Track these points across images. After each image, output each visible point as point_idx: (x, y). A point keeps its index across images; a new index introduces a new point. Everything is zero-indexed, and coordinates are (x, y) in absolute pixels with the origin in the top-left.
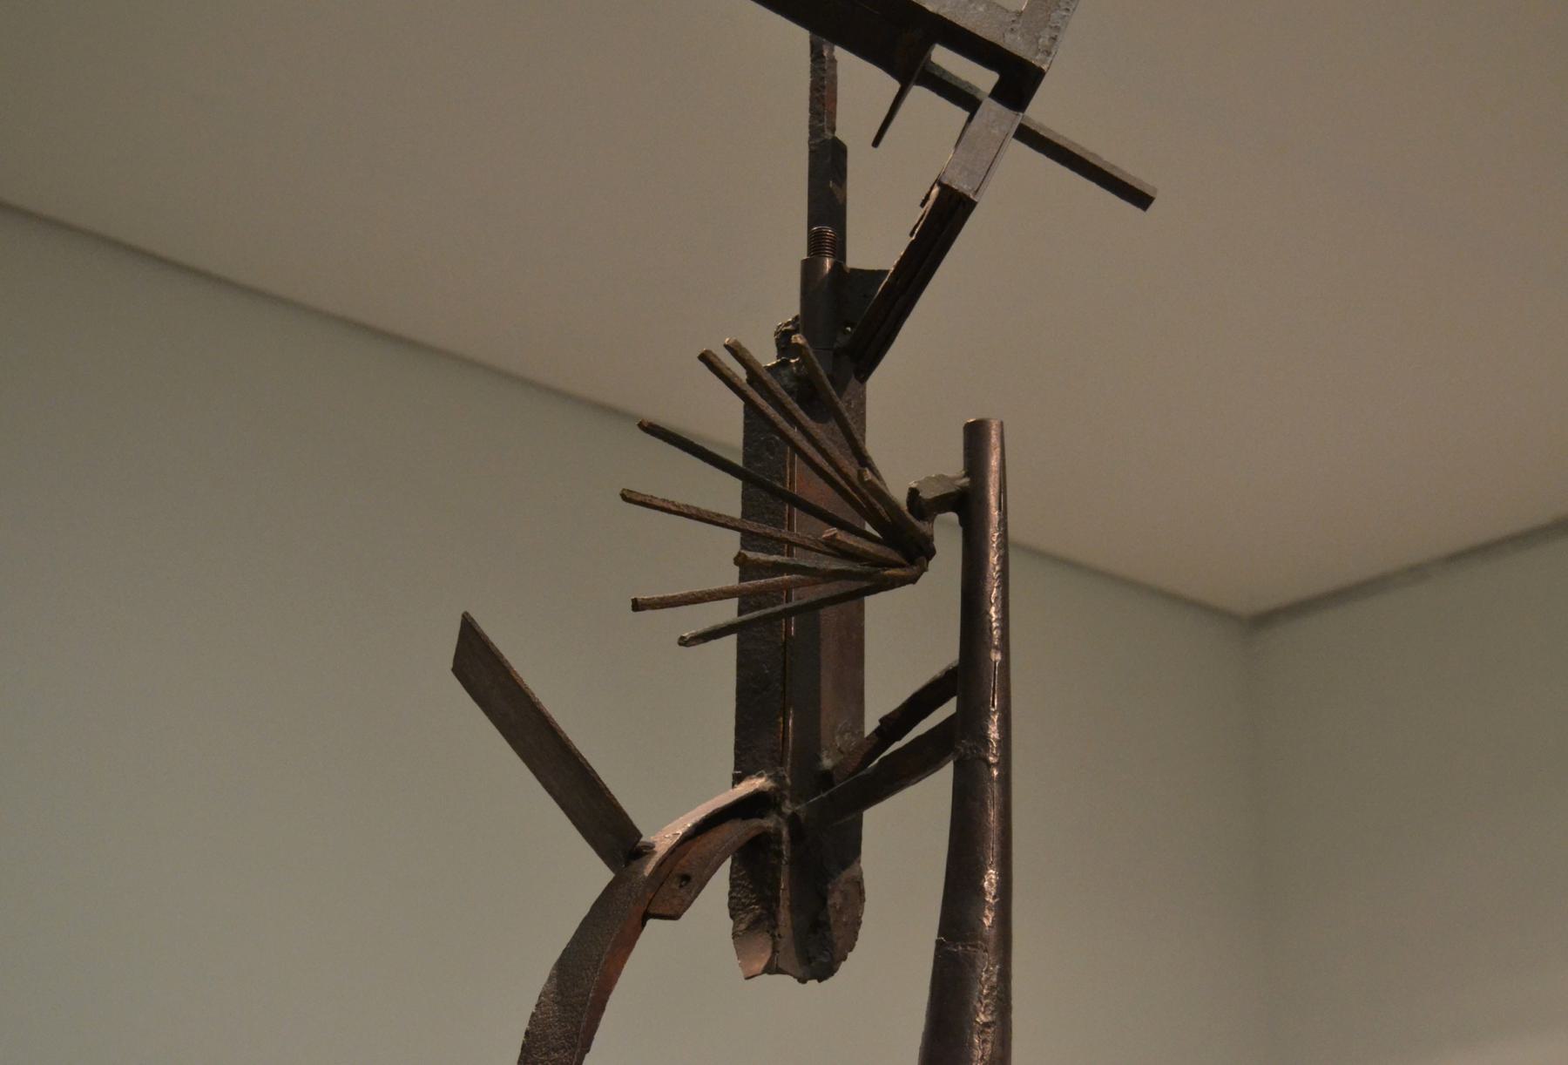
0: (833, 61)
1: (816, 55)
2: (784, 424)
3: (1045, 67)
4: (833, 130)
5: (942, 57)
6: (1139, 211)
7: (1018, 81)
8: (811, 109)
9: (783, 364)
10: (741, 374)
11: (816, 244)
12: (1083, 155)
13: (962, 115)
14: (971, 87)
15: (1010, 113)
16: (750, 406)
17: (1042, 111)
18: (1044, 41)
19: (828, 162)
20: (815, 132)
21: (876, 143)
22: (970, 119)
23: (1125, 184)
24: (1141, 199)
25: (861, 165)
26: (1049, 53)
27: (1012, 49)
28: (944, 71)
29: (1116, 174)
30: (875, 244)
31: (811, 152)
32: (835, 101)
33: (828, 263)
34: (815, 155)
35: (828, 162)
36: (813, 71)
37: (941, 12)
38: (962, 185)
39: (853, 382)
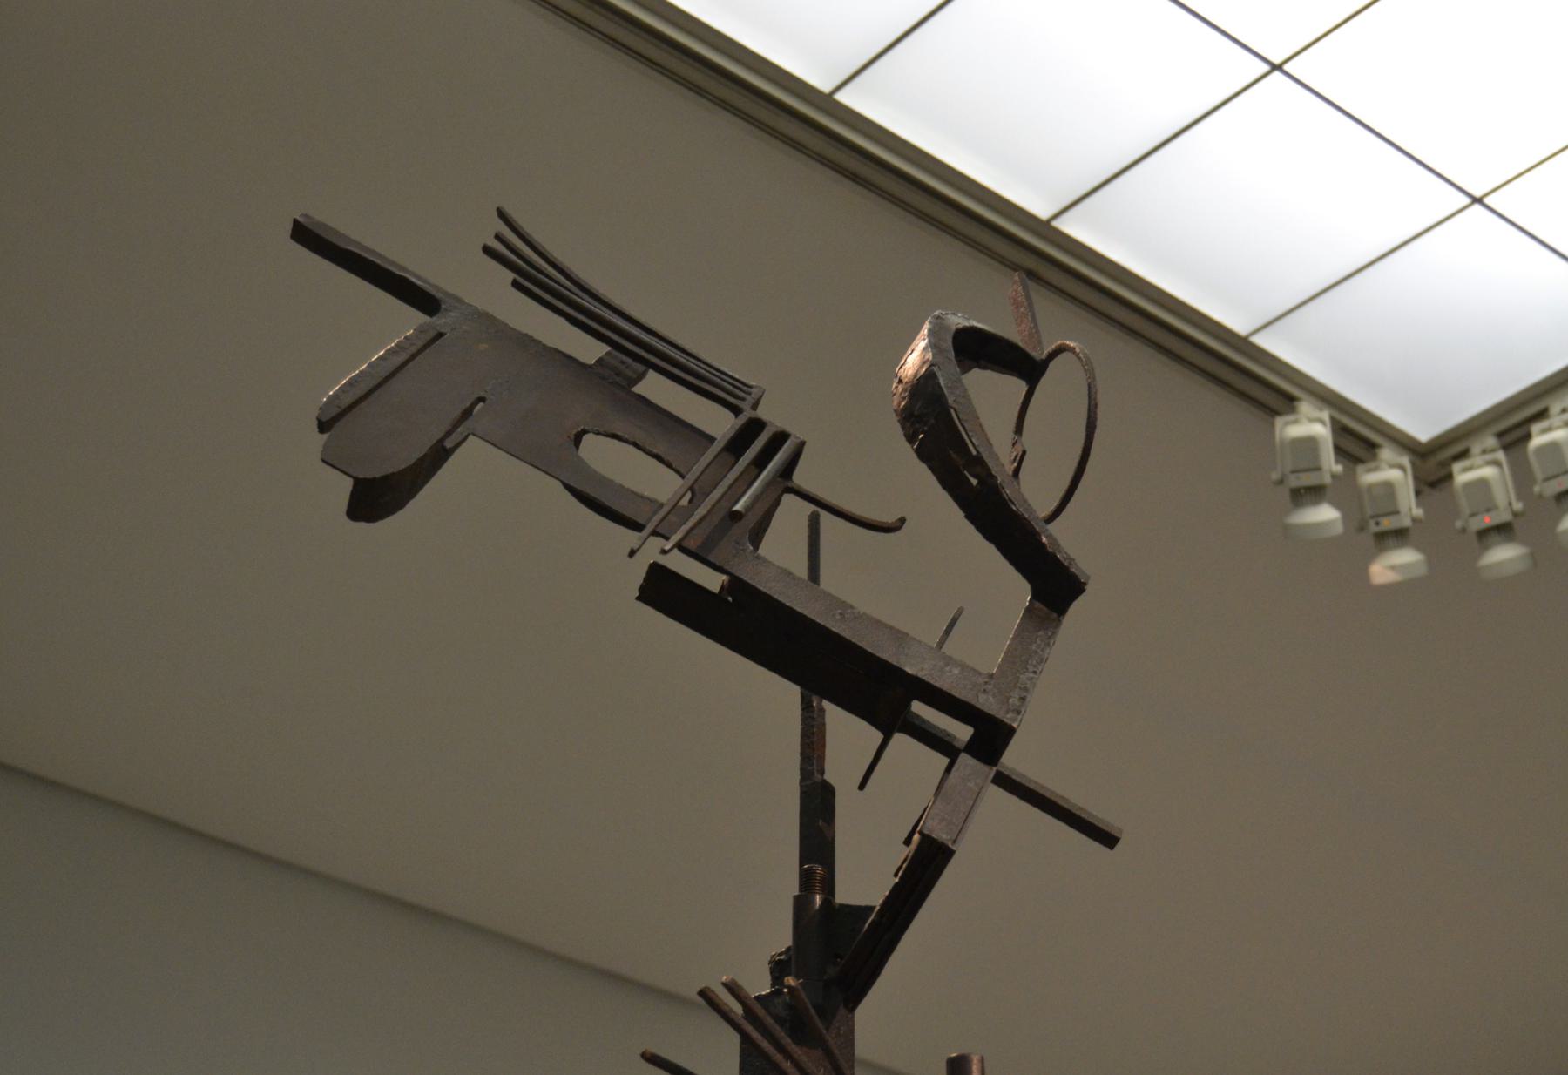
0: (822, 711)
1: (806, 706)
2: (778, 1057)
4: (822, 772)
5: (918, 708)
7: (991, 738)
8: (802, 754)
9: (777, 993)
10: (737, 1009)
11: (806, 880)
13: (1018, 386)
14: (948, 735)
15: (985, 768)
16: (745, 1038)
17: (1013, 759)
18: (1014, 701)
19: (817, 804)
20: (805, 774)
21: (862, 786)
22: (949, 769)
23: (1092, 825)
24: (1108, 839)
25: (847, 804)
26: (1019, 712)
27: (985, 709)
28: (924, 720)
30: (863, 880)
31: (802, 793)
32: (824, 746)
33: (818, 899)
34: (806, 795)
35: (817, 804)
36: (804, 720)
37: (920, 675)
38: (942, 835)
39: (842, 1011)
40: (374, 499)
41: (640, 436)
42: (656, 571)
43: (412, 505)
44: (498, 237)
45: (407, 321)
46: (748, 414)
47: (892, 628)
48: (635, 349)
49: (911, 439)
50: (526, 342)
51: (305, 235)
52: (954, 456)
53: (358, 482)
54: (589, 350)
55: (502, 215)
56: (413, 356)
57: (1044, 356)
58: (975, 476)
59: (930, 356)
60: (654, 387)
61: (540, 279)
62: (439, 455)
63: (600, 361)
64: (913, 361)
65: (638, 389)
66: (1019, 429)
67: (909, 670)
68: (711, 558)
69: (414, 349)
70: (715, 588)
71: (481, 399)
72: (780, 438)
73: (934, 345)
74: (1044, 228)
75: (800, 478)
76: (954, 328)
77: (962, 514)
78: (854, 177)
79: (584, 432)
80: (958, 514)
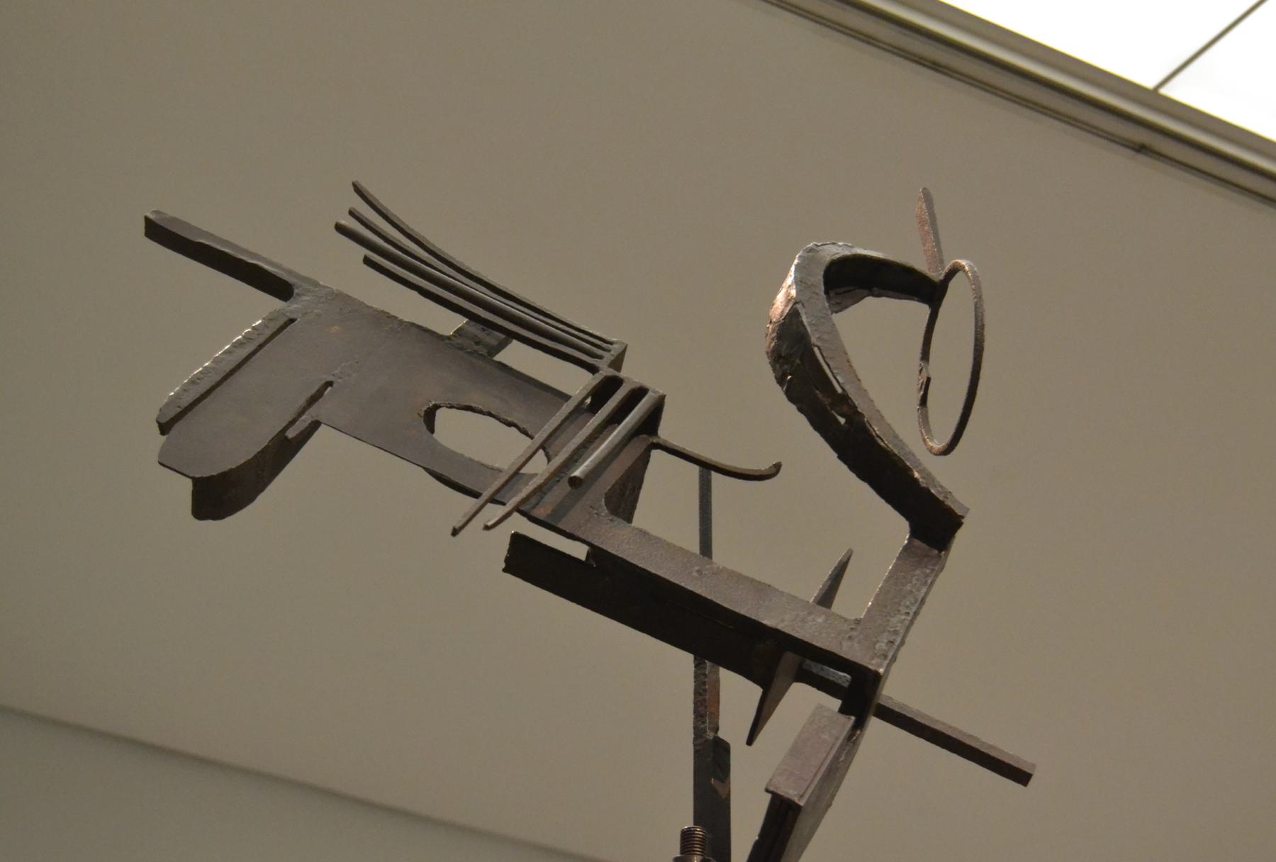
3: (881, 671)
4: (717, 729)
6: (1019, 787)
8: (696, 712)
10: (291, 434)
12: (960, 738)
18: (882, 645)
19: (712, 760)
20: (698, 733)
25: (740, 757)
29: (993, 754)
31: (696, 752)
35: (712, 760)
37: (780, 627)
40: (217, 497)
41: (494, 406)
42: (519, 542)
43: (261, 498)
44: (352, 213)
45: (258, 308)
46: (606, 371)
47: (753, 580)
48: (495, 319)
49: (781, 380)
50: (382, 319)
51: (157, 231)
52: (820, 396)
53: (196, 482)
54: (447, 323)
55: (358, 190)
56: (261, 346)
57: (942, 277)
58: (842, 416)
59: (793, 292)
60: (517, 356)
61: (398, 256)
62: (282, 450)
63: (459, 332)
64: (780, 305)
65: (498, 358)
66: (925, 355)
67: (764, 622)
68: (560, 526)
69: (262, 339)
70: (583, 557)
71: (330, 384)
72: (640, 392)
73: (799, 282)
74: (1151, 98)
75: (667, 431)
76: (828, 259)
77: (835, 455)
78: (935, 66)
79: (437, 407)
80: (833, 455)
